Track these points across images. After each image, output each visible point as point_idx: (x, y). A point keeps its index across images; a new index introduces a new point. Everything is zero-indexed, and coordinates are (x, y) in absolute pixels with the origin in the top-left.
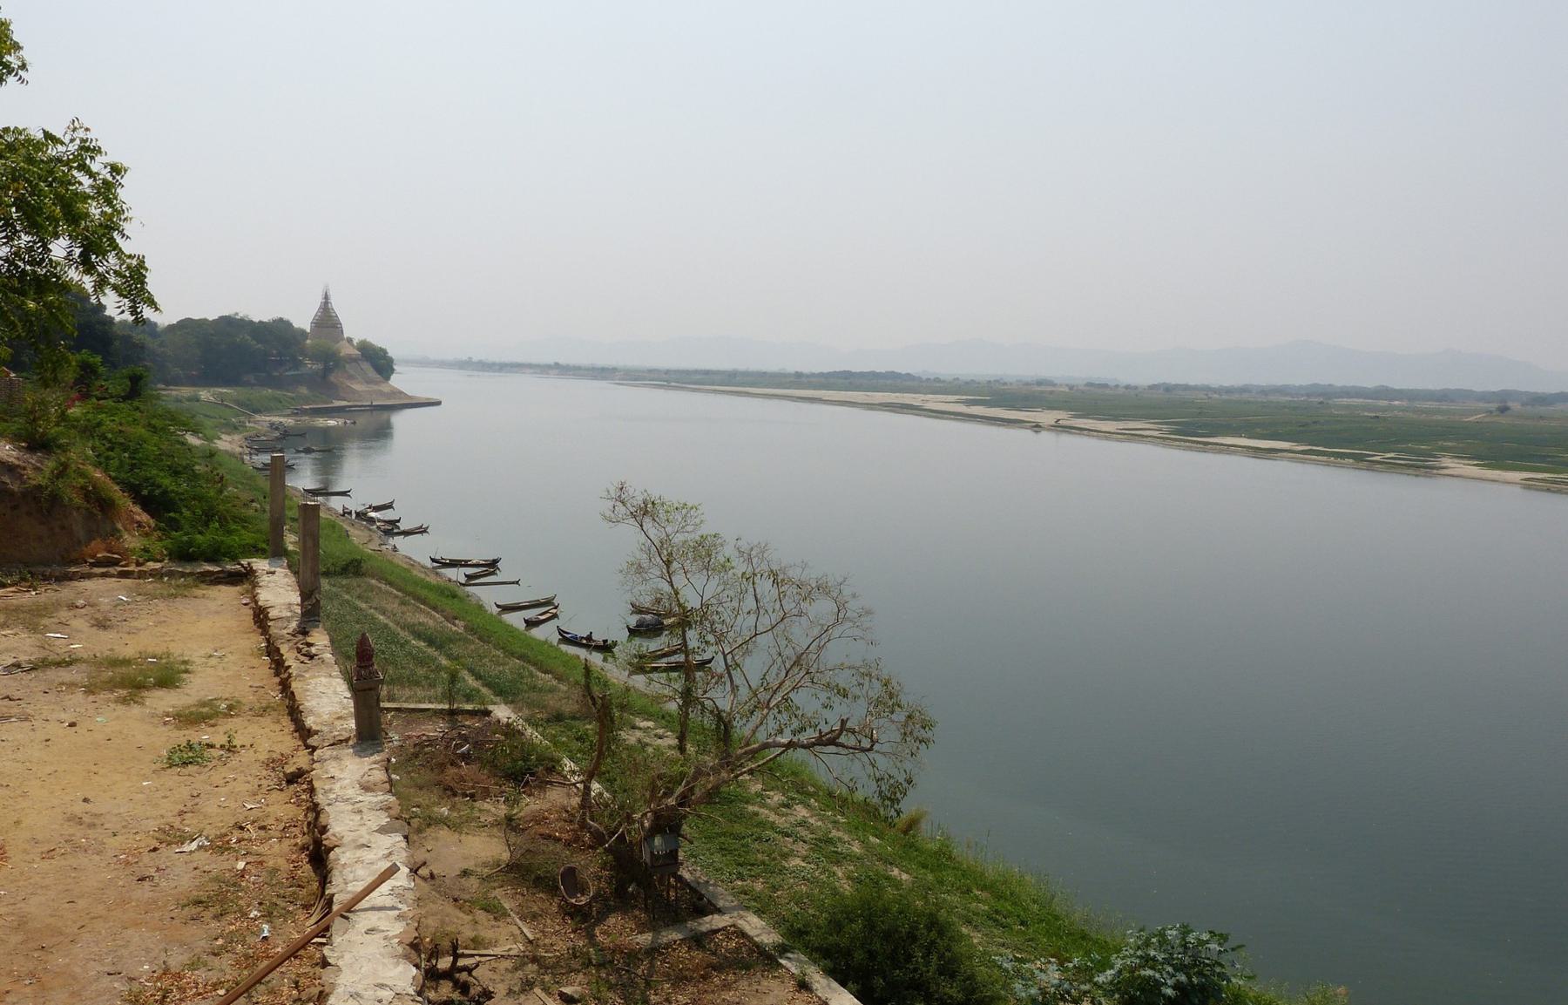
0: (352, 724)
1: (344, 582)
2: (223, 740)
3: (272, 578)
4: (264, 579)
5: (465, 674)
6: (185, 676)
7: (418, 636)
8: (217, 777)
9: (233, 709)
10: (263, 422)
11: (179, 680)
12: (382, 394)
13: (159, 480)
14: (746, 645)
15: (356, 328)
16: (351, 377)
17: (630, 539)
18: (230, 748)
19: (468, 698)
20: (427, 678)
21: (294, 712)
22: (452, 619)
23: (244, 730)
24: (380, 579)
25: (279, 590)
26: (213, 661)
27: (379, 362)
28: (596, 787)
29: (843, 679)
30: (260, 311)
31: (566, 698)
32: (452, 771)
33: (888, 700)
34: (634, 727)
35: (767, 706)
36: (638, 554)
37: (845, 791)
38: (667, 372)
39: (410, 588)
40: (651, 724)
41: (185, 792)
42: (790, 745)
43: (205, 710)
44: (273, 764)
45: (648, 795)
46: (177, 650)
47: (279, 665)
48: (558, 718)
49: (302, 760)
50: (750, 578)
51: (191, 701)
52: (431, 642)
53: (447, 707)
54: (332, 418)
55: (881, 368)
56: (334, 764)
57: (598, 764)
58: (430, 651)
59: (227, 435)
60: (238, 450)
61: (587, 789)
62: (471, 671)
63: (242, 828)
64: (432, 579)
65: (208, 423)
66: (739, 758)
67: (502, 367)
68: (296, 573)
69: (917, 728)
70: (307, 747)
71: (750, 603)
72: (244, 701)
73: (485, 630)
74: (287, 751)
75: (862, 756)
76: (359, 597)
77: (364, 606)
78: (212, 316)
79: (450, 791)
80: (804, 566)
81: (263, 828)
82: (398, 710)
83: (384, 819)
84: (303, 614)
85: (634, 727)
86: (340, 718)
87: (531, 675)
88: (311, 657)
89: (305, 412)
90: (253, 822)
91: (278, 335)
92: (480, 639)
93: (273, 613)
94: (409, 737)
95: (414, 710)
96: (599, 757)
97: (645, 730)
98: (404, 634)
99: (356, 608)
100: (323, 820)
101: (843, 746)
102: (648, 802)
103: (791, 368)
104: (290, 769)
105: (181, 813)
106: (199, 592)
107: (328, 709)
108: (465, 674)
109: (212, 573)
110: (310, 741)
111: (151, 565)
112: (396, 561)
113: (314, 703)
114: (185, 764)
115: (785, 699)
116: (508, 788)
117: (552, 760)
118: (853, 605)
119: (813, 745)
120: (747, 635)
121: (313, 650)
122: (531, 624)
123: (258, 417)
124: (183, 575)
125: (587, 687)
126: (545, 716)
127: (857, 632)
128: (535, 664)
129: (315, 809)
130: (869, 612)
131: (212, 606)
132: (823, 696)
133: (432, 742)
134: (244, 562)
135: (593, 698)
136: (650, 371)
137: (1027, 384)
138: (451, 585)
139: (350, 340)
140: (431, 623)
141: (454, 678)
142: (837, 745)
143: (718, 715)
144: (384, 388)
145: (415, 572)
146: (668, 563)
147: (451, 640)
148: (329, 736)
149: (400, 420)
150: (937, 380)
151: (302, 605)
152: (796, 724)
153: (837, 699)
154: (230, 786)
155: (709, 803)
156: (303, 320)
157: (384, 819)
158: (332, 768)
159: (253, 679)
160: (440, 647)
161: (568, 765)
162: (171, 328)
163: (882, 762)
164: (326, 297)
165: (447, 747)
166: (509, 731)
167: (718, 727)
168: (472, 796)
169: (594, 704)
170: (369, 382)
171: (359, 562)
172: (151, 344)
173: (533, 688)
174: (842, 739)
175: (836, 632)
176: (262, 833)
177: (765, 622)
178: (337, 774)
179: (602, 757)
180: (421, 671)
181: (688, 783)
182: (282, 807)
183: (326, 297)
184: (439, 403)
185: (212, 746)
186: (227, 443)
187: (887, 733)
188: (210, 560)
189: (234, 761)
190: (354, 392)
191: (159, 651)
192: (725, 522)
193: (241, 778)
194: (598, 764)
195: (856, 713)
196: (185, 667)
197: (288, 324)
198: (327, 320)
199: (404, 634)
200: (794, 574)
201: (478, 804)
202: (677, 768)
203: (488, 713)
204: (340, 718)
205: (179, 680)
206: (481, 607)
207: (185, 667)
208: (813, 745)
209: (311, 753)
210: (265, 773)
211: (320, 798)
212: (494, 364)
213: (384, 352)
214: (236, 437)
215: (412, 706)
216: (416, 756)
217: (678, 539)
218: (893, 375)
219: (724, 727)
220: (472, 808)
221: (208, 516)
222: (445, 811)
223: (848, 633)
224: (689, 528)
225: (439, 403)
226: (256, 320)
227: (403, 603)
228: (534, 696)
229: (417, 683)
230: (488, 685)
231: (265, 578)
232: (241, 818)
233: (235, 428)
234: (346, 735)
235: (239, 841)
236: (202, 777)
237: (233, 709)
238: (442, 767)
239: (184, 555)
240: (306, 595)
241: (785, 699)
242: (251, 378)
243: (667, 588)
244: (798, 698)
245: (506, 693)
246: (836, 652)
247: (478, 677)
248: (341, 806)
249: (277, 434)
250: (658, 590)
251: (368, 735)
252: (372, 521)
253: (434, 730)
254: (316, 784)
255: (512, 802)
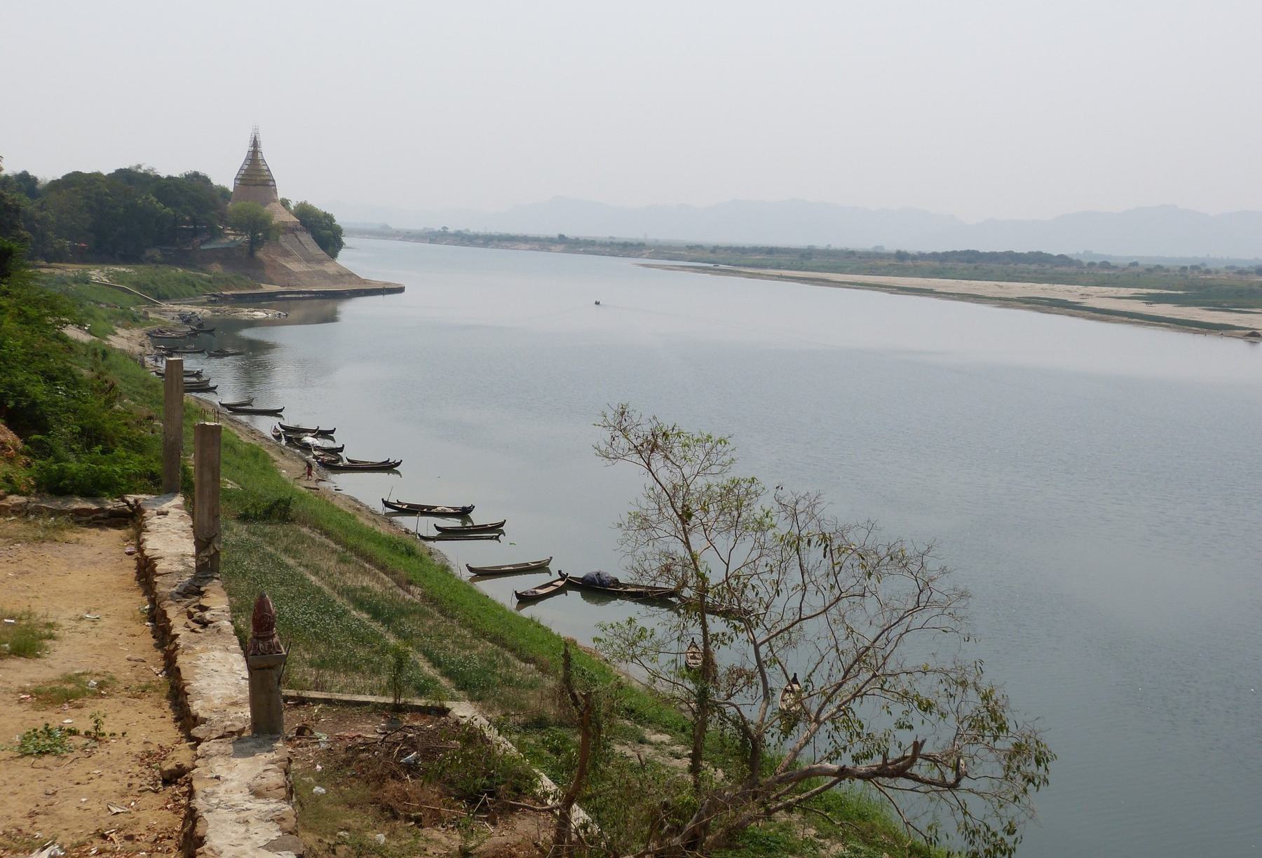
0: (247, 712)
1: (268, 529)
2: (88, 725)
3: (164, 520)
4: (153, 521)
5: (416, 656)
6: (48, 642)
7: (360, 604)
8: (78, 772)
9: (104, 687)
10: (170, 312)
11: (41, 647)
12: (325, 276)
13: (28, 388)
14: (788, 631)
15: (294, 186)
16: (287, 254)
17: (632, 483)
18: (96, 736)
19: (422, 691)
20: (369, 661)
21: (177, 695)
22: (405, 584)
23: (116, 714)
24: (316, 526)
25: (170, 535)
26: (85, 626)
27: (322, 232)
28: (579, 815)
29: (926, 687)
30: (169, 163)
31: (542, 695)
32: (392, 785)
33: (991, 720)
34: (642, 741)
35: (817, 720)
36: (645, 503)
37: (921, 841)
38: (715, 249)
39: (352, 541)
40: (666, 738)
41: (39, 788)
42: (843, 773)
43: (70, 687)
44: (149, 758)
45: (647, 829)
46: (39, 609)
47: (163, 635)
48: (539, 723)
49: (183, 755)
50: (795, 543)
51: (51, 674)
52: (376, 614)
53: (390, 700)
54: (260, 308)
55: (1022, 248)
56: (221, 761)
57: (578, 786)
58: (376, 626)
59: (117, 327)
60: (138, 349)
61: (565, 820)
62: (428, 655)
63: (104, 837)
64: (383, 530)
65: (103, 310)
66: (771, 787)
67: (489, 241)
68: (192, 515)
69: (1028, 761)
70: (190, 738)
71: (795, 576)
72: (120, 677)
73: (450, 602)
74: (167, 744)
75: (948, 794)
76: (286, 550)
77: (291, 562)
78: (107, 169)
79: (389, 813)
80: (871, 527)
81: (130, 838)
82: (328, 702)
83: (274, 833)
84: (198, 569)
85: (642, 741)
86: (234, 704)
87: (507, 663)
88: (205, 624)
89: (225, 299)
90: (119, 830)
91: (191, 193)
92: (442, 612)
93: (161, 566)
94: (341, 738)
95: (348, 703)
96: (580, 777)
97: (658, 746)
98: (341, 601)
99: (281, 565)
100: (199, 830)
101: (915, 778)
102: (646, 840)
103: (891, 244)
104: (168, 766)
105: (32, 815)
106: (69, 535)
107: (220, 692)
108: (416, 656)
109: (89, 511)
110: (196, 732)
111: (14, 499)
112: (336, 503)
113: (203, 683)
114: (41, 753)
115: (843, 709)
116: (461, 810)
117: (519, 776)
118: (942, 586)
119: (875, 774)
120: (789, 617)
121: (208, 615)
122: (525, 599)
123: (165, 305)
124: (53, 513)
125: (567, 680)
126: (521, 720)
127: (945, 621)
128: (512, 650)
129: (192, 816)
130: (963, 595)
131: (87, 553)
132: (898, 709)
133: (369, 746)
134: (131, 498)
135: (574, 696)
136: (690, 248)
137: (1241, 272)
138: (408, 538)
139: (285, 203)
140: (378, 588)
141: (400, 664)
142: (907, 777)
143: (742, 725)
144: (329, 268)
145: (361, 520)
146: (686, 516)
147: (402, 613)
148: (219, 726)
149: (350, 309)
150: (1105, 265)
151: (197, 556)
152: (858, 747)
153: (916, 716)
154: (94, 784)
155: (729, 847)
156: (224, 176)
157: (274, 833)
158: (219, 766)
159: (130, 650)
160: (387, 621)
161: (547, 783)
162: (55, 185)
163: (978, 807)
164: (255, 144)
165: (388, 754)
166: (472, 736)
167: (743, 742)
168: (418, 820)
169: (576, 703)
170: (309, 259)
171: (287, 503)
172: (28, 205)
173: (509, 681)
174: (915, 770)
175: (918, 620)
176: (128, 844)
177: (815, 602)
178: (223, 775)
179: (581, 777)
180: (362, 653)
181: (700, 818)
182: (155, 814)
183: (255, 144)
184: (400, 290)
185: (73, 732)
186: (124, 340)
187: (985, 765)
188: (87, 494)
189: (101, 753)
190: (289, 273)
191: (18, 610)
192: (767, 464)
193: (108, 774)
194: (578, 786)
195: (937, 735)
196: (50, 631)
197: (206, 180)
198: (255, 175)
199: (341, 601)
200: (856, 538)
201: (424, 832)
202: (686, 796)
203: (444, 712)
204: (234, 704)
205: (41, 647)
206: (446, 569)
207: (50, 631)
208: (875, 774)
209: (194, 748)
210: (137, 769)
211: (199, 803)
212: (477, 237)
213: (329, 218)
214: (137, 332)
215: (346, 697)
216: (348, 762)
217: (700, 483)
218: (1039, 258)
219: (749, 748)
220: (417, 836)
221: (91, 436)
222: (381, 838)
223: (935, 622)
224: (715, 469)
225: (400, 290)
226: (164, 174)
227: (342, 560)
228: (509, 692)
229: (356, 668)
230: (448, 674)
231: (155, 520)
232: (104, 824)
233: (134, 321)
234: (239, 726)
235: (100, 852)
236: (61, 771)
237: (104, 687)
238: (380, 780)
239: (56, 486)
240: (203, 543)
241: (843, 709)
242: (156, 253)
243: (681, 551)
244: (865, 710)
245: (469, 686)
246: (913, 651)
247: (436, 663)
248: (223, 813)
249: (187, 329)
250: (669, 555)
251: (264, 727)
252: (307, 448)
253: (371, 730)
254: (197, 785)
255: (468, 834)
